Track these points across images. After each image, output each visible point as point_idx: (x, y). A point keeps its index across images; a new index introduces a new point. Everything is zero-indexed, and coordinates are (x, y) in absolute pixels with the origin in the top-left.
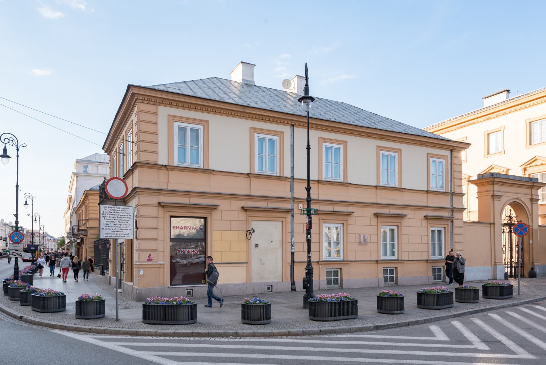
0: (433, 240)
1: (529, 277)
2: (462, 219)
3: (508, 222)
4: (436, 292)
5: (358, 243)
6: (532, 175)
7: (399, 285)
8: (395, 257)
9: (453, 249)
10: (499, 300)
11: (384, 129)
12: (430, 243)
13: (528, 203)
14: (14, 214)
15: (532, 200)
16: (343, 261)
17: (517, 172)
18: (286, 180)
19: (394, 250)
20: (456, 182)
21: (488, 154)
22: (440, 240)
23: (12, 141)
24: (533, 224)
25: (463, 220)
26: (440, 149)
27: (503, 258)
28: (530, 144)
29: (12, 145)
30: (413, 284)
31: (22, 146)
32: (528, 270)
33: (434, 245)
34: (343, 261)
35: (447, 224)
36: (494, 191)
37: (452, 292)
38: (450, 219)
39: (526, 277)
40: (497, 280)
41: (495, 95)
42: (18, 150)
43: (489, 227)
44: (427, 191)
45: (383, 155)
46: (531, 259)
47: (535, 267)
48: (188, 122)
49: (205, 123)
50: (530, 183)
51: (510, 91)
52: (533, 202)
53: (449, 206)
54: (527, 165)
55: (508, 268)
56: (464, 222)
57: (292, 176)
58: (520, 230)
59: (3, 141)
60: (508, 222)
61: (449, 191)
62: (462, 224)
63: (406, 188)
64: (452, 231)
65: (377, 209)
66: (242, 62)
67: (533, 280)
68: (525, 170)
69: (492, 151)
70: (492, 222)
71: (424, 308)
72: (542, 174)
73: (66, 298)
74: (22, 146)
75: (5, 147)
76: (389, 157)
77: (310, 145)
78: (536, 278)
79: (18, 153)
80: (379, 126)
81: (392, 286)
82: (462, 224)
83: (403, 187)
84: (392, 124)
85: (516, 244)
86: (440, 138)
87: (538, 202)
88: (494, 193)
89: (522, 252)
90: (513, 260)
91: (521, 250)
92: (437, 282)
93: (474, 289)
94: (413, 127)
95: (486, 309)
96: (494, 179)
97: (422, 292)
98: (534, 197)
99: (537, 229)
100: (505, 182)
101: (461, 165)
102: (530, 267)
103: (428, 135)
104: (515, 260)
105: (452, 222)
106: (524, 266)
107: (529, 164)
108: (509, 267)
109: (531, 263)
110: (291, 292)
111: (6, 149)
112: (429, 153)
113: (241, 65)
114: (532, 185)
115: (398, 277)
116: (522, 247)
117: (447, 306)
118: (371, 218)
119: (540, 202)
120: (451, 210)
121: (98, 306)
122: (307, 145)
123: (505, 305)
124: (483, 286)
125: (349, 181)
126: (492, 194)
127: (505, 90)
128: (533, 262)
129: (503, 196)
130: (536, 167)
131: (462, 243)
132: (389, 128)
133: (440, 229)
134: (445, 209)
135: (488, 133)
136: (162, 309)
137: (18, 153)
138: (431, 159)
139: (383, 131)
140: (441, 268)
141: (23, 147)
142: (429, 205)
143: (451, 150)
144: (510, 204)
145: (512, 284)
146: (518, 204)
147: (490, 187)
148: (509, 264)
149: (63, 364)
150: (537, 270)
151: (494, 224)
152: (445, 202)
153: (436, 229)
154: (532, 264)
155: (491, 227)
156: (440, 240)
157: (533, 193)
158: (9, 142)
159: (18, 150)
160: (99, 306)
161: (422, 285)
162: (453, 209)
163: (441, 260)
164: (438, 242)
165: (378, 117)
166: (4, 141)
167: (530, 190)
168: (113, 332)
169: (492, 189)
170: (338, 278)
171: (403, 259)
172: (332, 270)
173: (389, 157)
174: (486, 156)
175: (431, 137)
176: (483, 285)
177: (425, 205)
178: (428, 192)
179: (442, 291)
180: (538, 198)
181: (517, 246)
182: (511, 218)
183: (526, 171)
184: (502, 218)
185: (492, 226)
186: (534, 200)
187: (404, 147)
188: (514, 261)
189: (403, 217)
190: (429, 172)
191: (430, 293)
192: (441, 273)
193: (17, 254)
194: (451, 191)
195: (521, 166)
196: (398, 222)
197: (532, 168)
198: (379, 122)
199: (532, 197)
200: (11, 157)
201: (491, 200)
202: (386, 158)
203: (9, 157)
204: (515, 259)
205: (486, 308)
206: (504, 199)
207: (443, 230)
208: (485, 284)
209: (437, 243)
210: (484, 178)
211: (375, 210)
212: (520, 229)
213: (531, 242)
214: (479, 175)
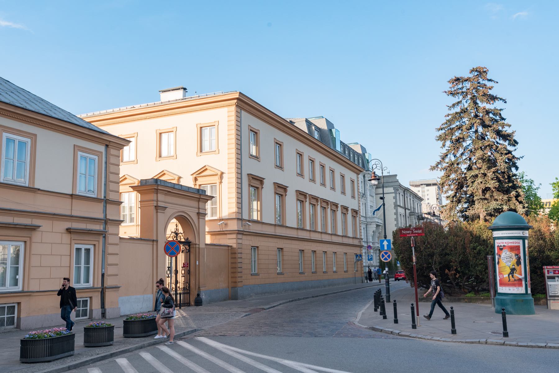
0: (78, 262)
1: (195, 306)
2: (118, 234)
3: (173, 239)
4: (48, 336)
6: (202, 186)
7: (22, 329)
8: (19, 288)
9: (104, 274)
10: (141, 338)
11: (11, 103)
12: (74, 265)
13: (195, 217)
15: (198, 214)
16: (22, 292)
17: (188, 182)
18: (37, 192)
19: (17, 278)
20: (112, 186)
21: (160, 156)
22: (87, 262)
24: (199, 242)
25: (119, 235)
26: (91, 142)
27: (167, 284)
28: (201, 151)
30: (43, 326)
32: (194, 297)
33: (79, 269)
35: (98, 240)
36: (157, 201)
37: (73, 334)
38: (102, 234)
39: (192, 305)
41: (172, 90)
43: (152, 246)
44: (72, 196)
45: (82, 157)
46: (197, 283)
47: (201, 292)
49: (33, 137)
50: (197, 195)
51: (187, 89)
52: (200, 217)
53: (101, 216)
54: (198, 174)
55: (185, 295)
56: (120, 238)
57: (105, 197)
58: (172, 249)
60: (173, 239)
61: (103, 198)
62: (117, 241)
63: (41, 188)
64: (104, 250)
65: (71, 223)
67: (198, 308)
68: (196, 179)
69: (164, 154)
70: (155, 239)
71: (29, 362)
72: (211, 186)
76: (17, 142)
78: (202, 305)
80: (5, 97)
81: (10, 331)
82: (117, 241)
83: (36, 187)
84: (28, 99)
85: (182, 266)
86: (93, 129)
87: (205, 217)
89: (188, 275)
90: (178, 285)
91: (188, 272)
92: (81, 319)
93: (107, 326)
94: (59, 108)
95: (117, 352)
96: (158, 187)
97: (27, 338)
98: (201, 211)
99: (204, 249)
100: (170, 192)
101: (119, 165)
102: (196, 293)
103: (31, 106)
104: (181, 285)
105: (105, 237)
106: (191, 292)
107: (199, 174)
108: (174, 294)
109: (197, 288)
112: (76, 146)
114: (199, 197)
115: (21, 316)
116: (188, 269)
117: (62, 354)
118: (63, 234)
119: (208, 218)
120: (104, 222)
123: (144, 344)
124: (124, 321)
125: (36, 186)
127: (182, 87)
128: (199, 287)
129: (167, 207)
130: (206, 177)
131: (117, 265)
132: (20, 104)
133: (88, 247)
134: (96, 221)
135: (161, 132)
136: (28, 345)
138: (80, 153)
139: (8, 106)
140: (87, 301)
142: (74, 214)
143: (107, 146)
144: (175, 218)
146: (185, 219)
147: (153, 196)
148: (174, 291)
150: (203, 297)
151: (157, 241)
152: (96, 211)
153: (83, 247)
154: (198, 289)
155: (153, 245)
156: (87, 262)
157: (200, 207)
161: (115, 318)
162: (106, 221)
163: (88, 289)
164: (84, 265)
165: (10, 86)
167: (197, 203)
169: (155, 199)
170: (14, 317)
171: (30, 290)
172: (6, 306)
173: (17, 142)
174: (158, 159)
175: (80, 124)
176: (125, 320)
177: (68, 213)
178: (73, 196)
179: (57, 334)
180: (206, 212)
181: (183, 268)
182: (177, 234)
183: (197, 181)
184: (166, 234)
185: (155, 243)
186: (201, 215)
187: (43, 134)
188: (179, 287)
189: (35, 229)
190: (77, 170)
191: (39, 338)
192: (87, 307)
194: (105, 197)
195: (192, 175)
196: (92, 239)
197: (202, 178)
198: (8, 92)
199: (199, 211)
201: (155, 211)
202: (13, 144)
204: (180, 284)
205: (117, 351)
206: (169, 212)
207: (92, 248)
208: (126, 319)
209: (83, 266)
210: (147, 184)
211: (68, 225)
212: (172, 248)
213: (197, 264)
214: (142, 181)
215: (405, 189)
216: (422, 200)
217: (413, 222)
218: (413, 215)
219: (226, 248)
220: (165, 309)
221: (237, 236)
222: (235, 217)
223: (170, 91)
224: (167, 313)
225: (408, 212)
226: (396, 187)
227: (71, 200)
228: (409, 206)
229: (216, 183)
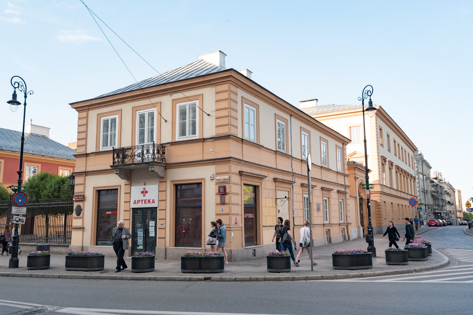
5: (316, 210)
14: (17, 172)
23: (21, 86)
29: (21, 91)
31: (29, 93)
34: (344, 224)
40: (361, 238)
42: (26, 97)
48: (249, 104)
54: (350, 156)
59: (13, 84)
66: (220, 51)
74: (29, 93)
75: (15, 92)
77: (24, 105)
79: (25, 101)
88: (355, 176)
107: (351, 156)
110: (8, 268)
111: (16, 94)
113: (219, 53)
115: (331, 237)
122: (364, 139)
126: (354, 176)
137: (25, 101)
141: (30, 94)
158: (18, 87)
159: (26, 97)
168: (343, 277)
193: (20, 219)
200: (7, 102)
203: (19, 103)
212: (17, 195)
215: (423, 161)
216: (431, 168)
217: (428, 184)
218: (428, 179)
219: (374, 202)
220: (211, 237)
221: (380, 195)
222: (378, 183)
223: (307, 101)
224: (211, 240)
225: (424, 177)
226: (418, 159)
227: (336, 175)
228: (425, 173)
229: (363, 162)
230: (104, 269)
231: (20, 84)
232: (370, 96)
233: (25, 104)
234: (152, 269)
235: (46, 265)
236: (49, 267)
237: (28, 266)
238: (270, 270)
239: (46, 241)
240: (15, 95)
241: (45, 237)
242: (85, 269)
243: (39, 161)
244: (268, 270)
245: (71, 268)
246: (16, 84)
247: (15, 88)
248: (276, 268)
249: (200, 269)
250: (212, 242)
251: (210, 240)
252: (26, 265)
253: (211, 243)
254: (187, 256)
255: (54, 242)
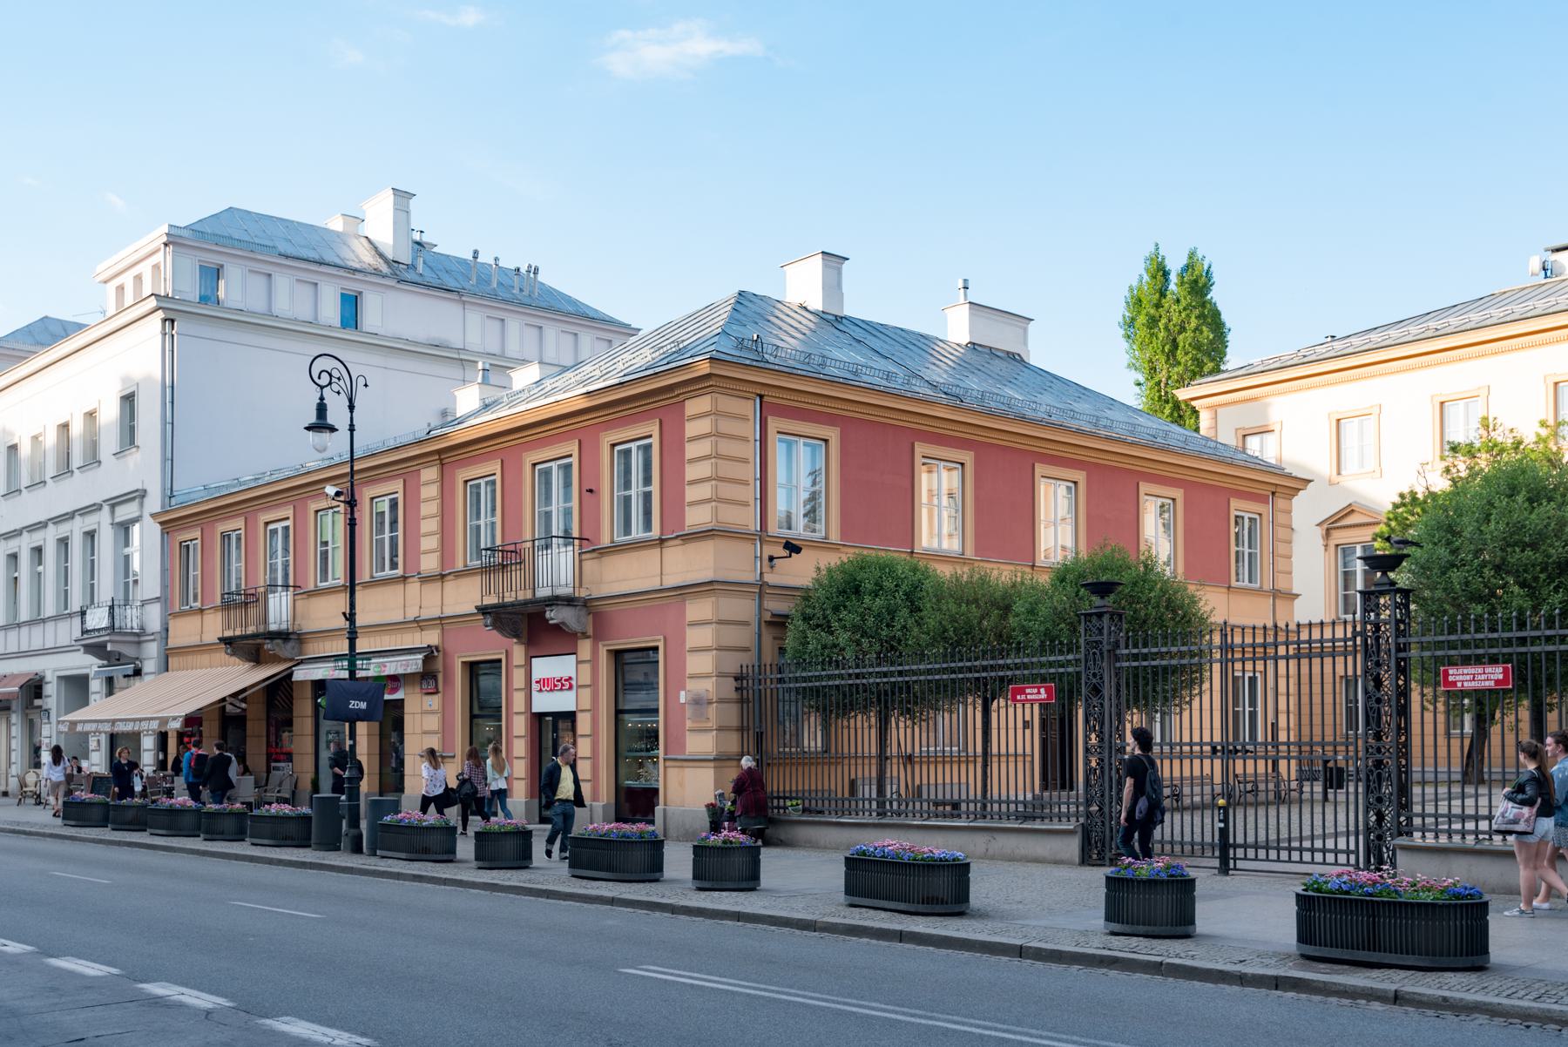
29: (339, 393)
54: (1333, 523)
59: (315, 377)
73: (969, 872)
75: (322, 398)
111: (325, 405)
121: (1462, 925)
145: (1191, 877)
149: (1412, 1045)
158: (330, 383)
160: (1464, 923)
166: (319, 378)
176: (848, 855)
203: (332, 429)
220: (1511, 804)
224: (1511, 817)
230: (1488, 965)
231: (336, 374)
232: (322, 388)
233: (352, 429)
234: (1477, 960)
235: (1471, 953)
236: (968, 907)
237: (696, 877)
238: (1310, 950)
239: (880, 810)
240: (322, 409)
241: (892, 794)
242: (902, 906)
243: (1081, 455)
244: (1105, 927)
245: (875, 901)
246: (325, 375)
247: (322, 388)
248: (1135, 920)
249: (1373, 946)
250: (1515, 821)
251: (1507, 815)
252: (691, 876)
253: (1510, 827)
254: (622, 837)
255: (867, 814)
